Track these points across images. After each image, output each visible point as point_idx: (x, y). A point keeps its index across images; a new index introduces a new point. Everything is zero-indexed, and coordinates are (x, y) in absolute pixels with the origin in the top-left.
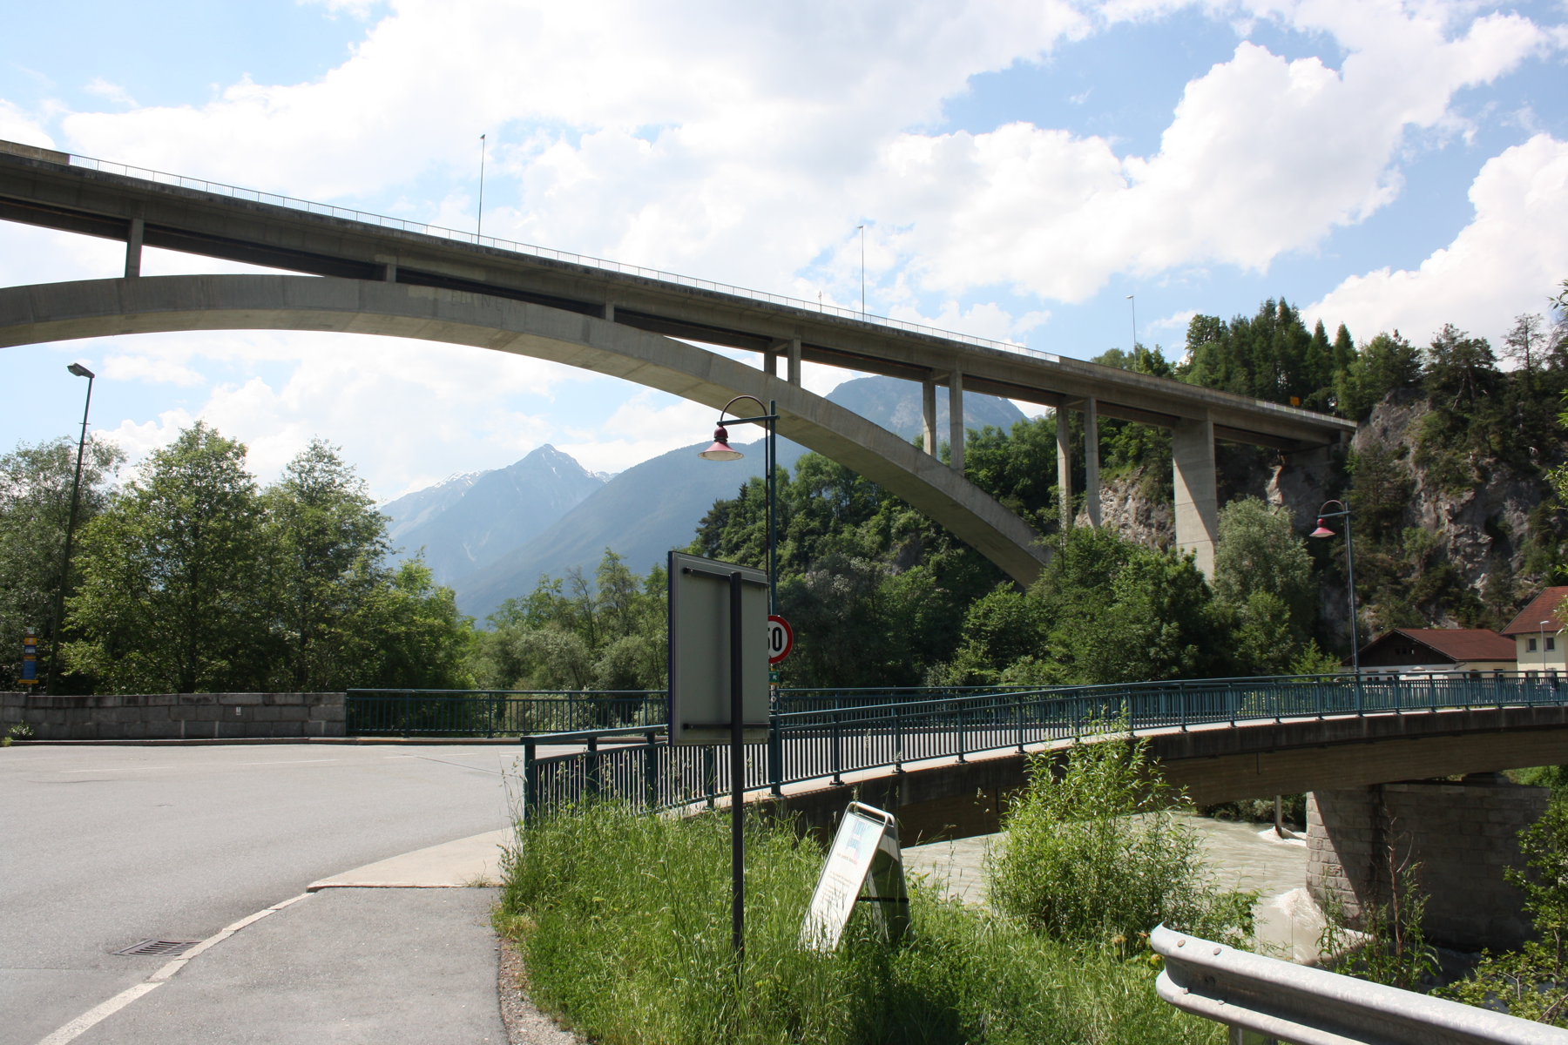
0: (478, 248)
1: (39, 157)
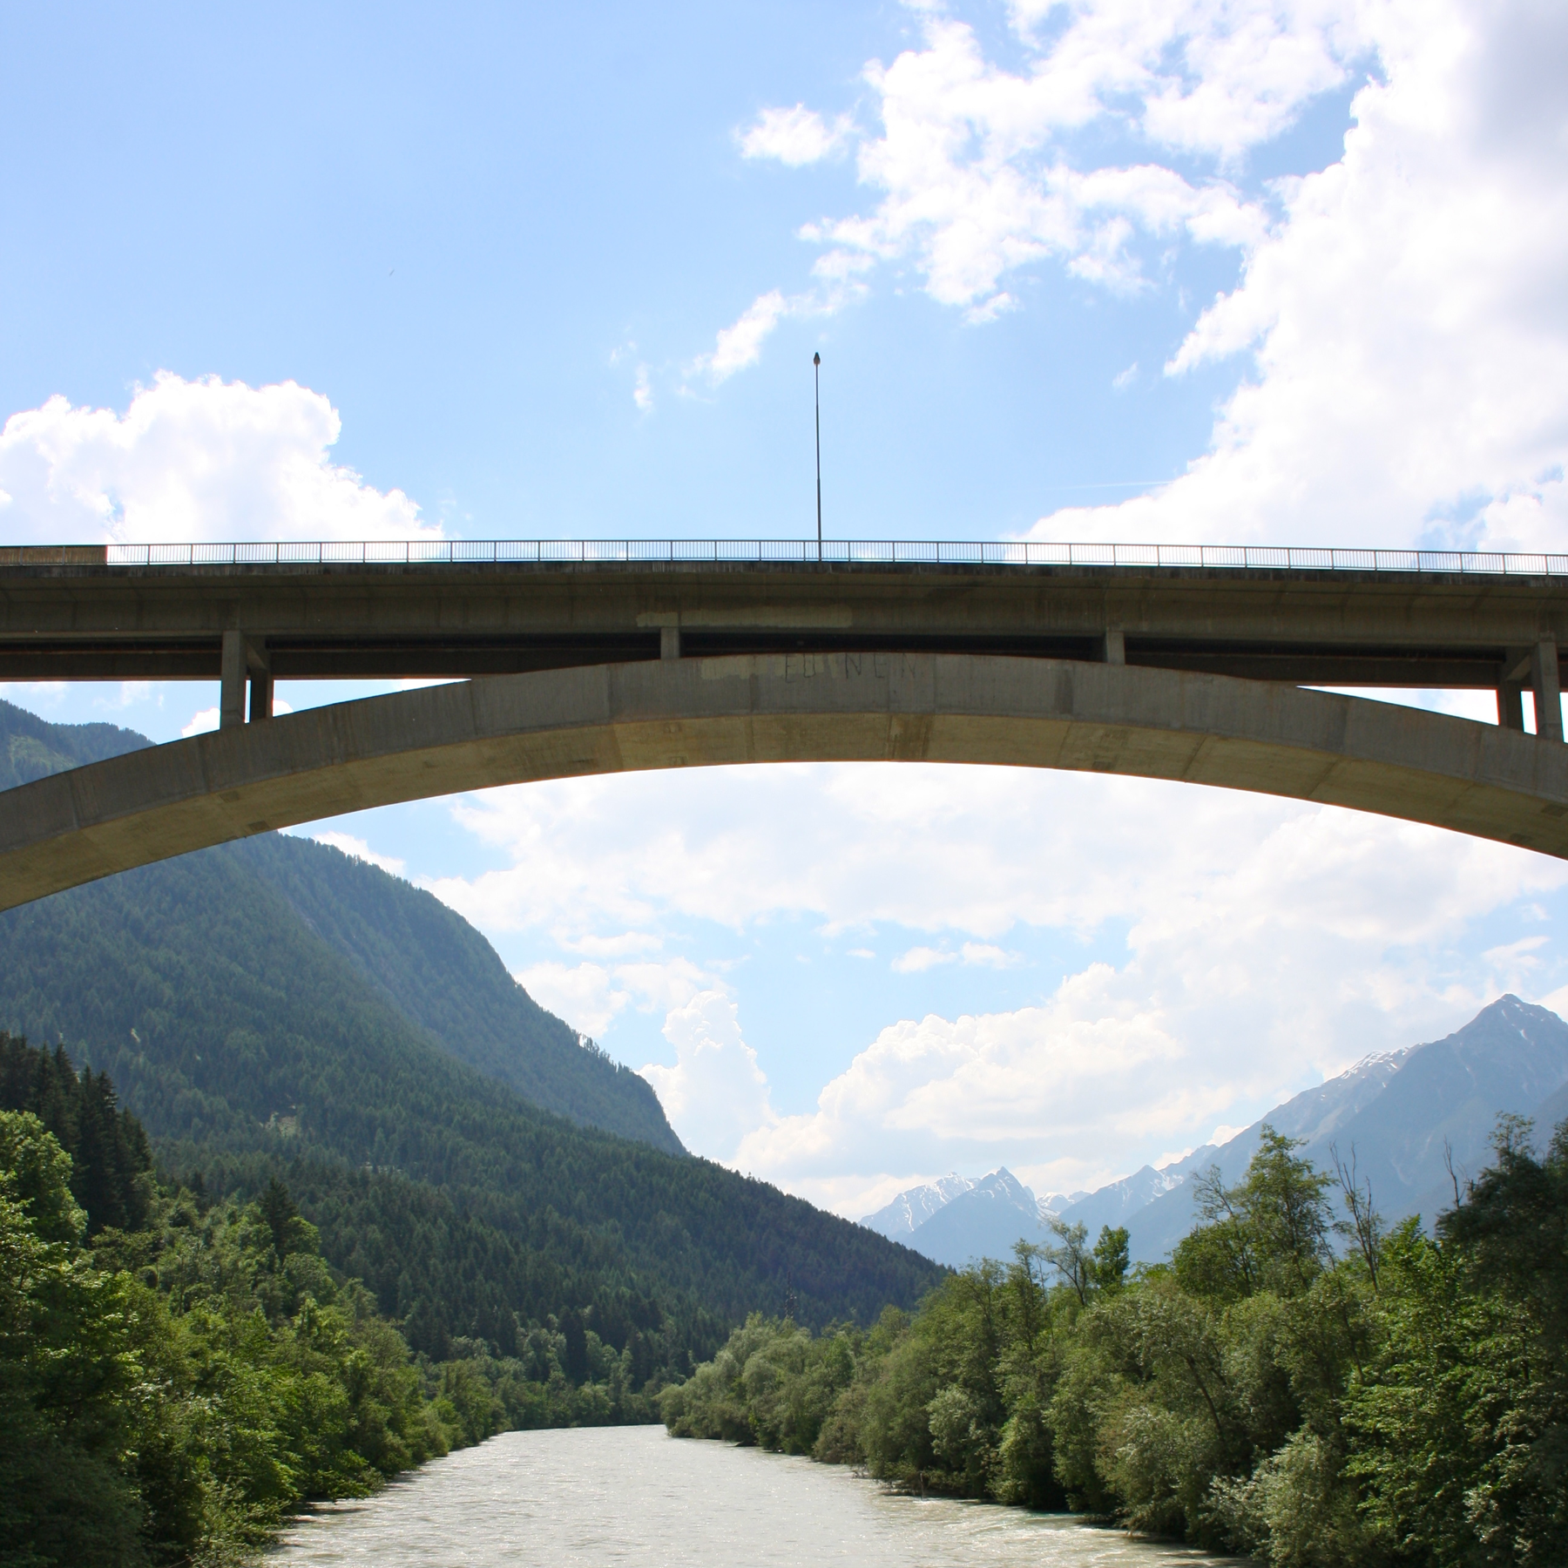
0: (819, 566)
1: (61, 560)
